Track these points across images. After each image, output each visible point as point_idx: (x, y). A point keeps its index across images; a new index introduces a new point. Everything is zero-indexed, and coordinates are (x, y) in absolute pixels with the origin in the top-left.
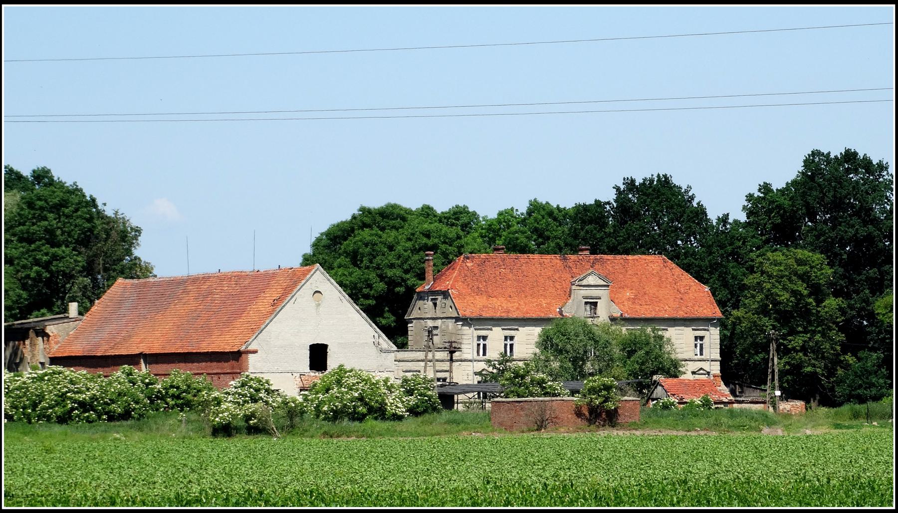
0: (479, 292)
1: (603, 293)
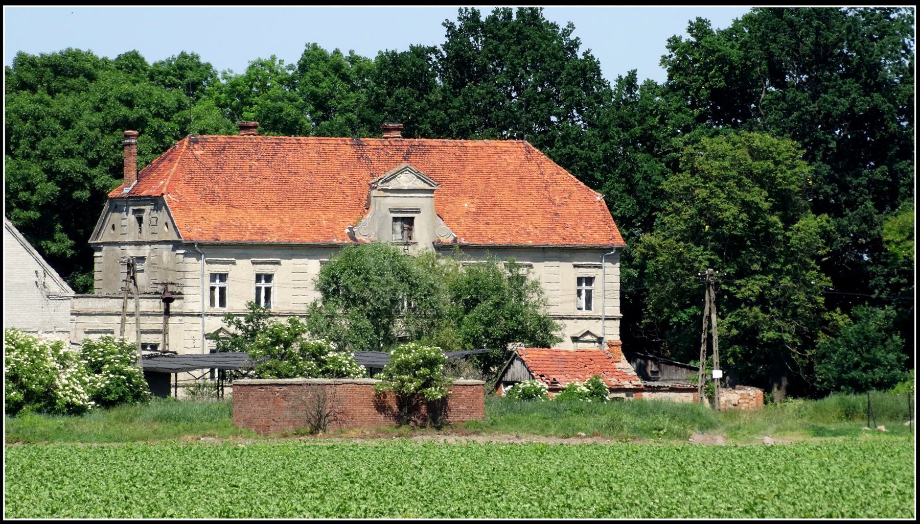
0: (212, 199)
1: (423, 202)
